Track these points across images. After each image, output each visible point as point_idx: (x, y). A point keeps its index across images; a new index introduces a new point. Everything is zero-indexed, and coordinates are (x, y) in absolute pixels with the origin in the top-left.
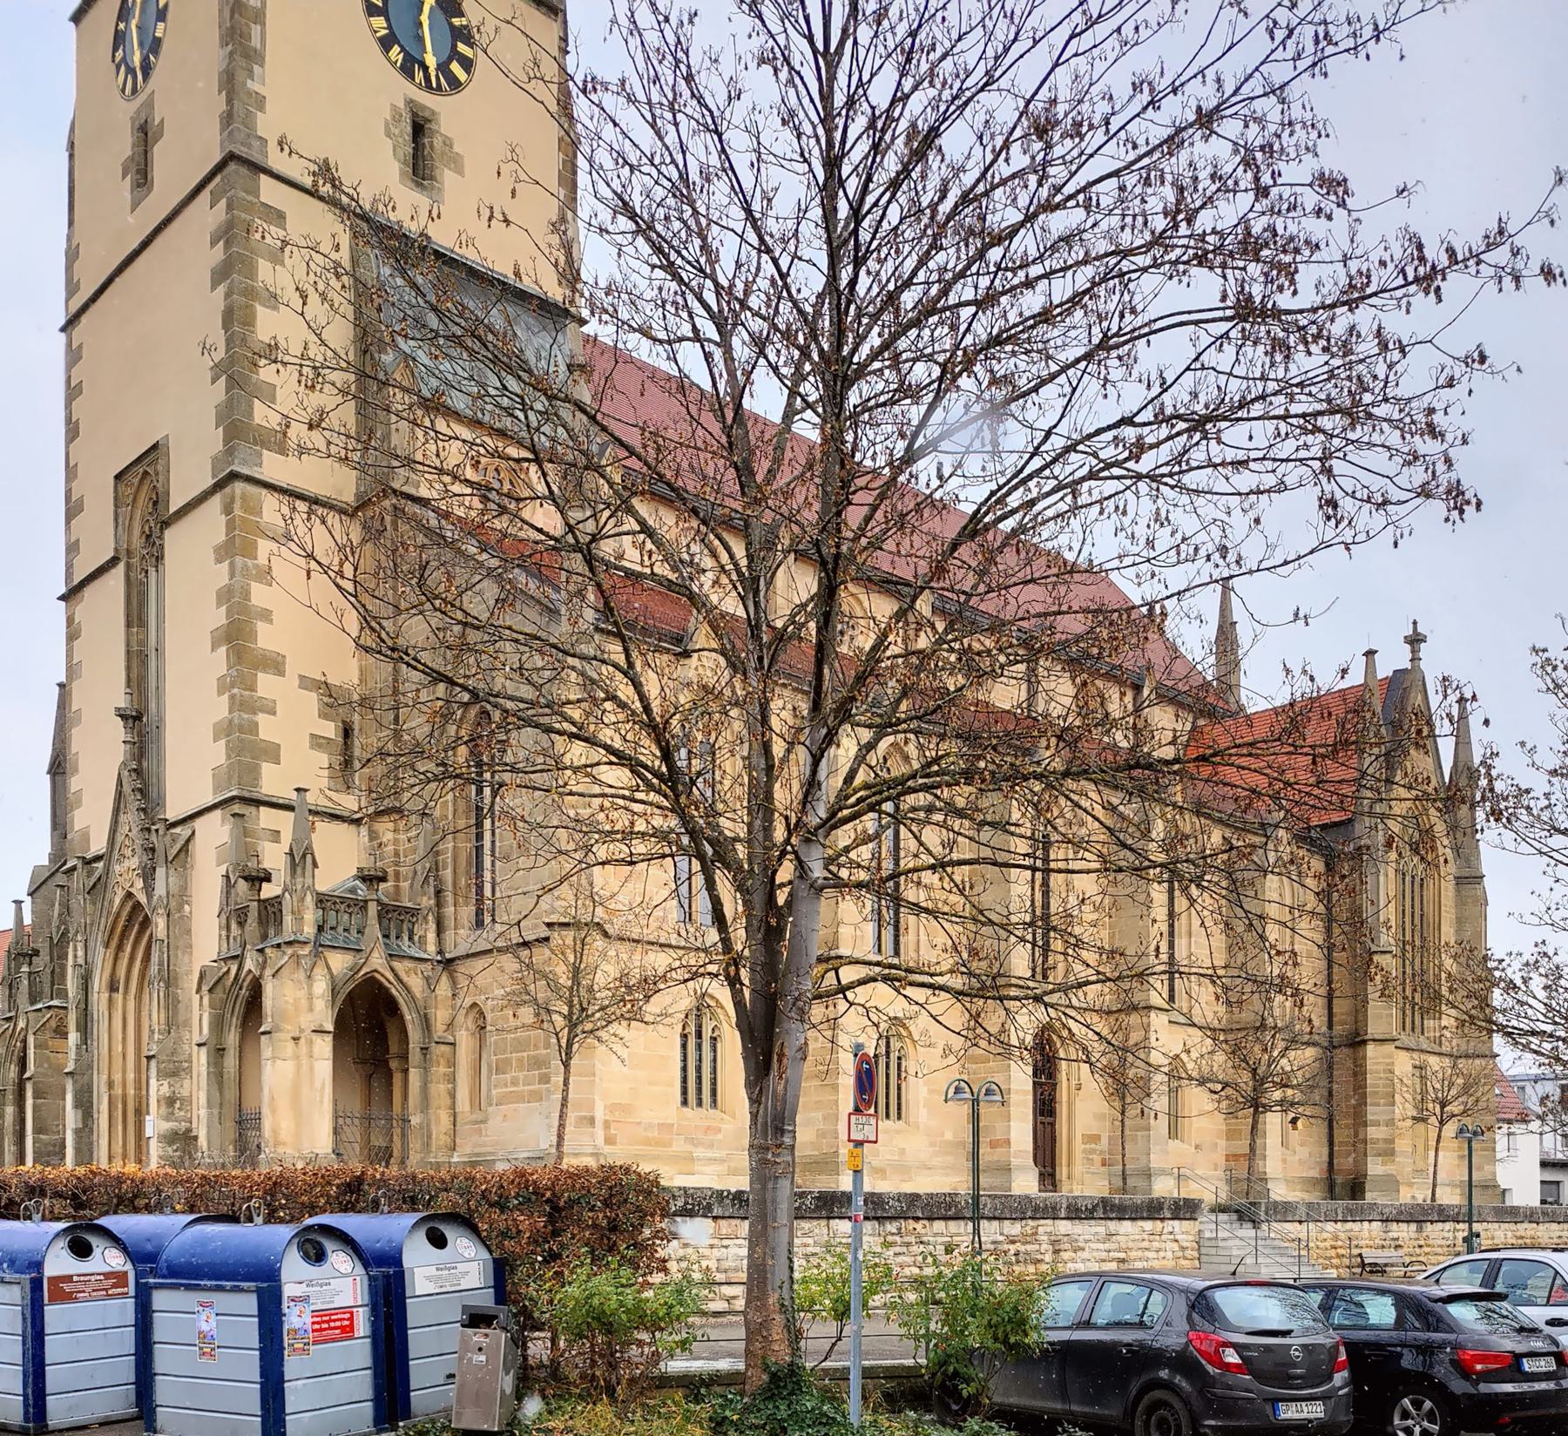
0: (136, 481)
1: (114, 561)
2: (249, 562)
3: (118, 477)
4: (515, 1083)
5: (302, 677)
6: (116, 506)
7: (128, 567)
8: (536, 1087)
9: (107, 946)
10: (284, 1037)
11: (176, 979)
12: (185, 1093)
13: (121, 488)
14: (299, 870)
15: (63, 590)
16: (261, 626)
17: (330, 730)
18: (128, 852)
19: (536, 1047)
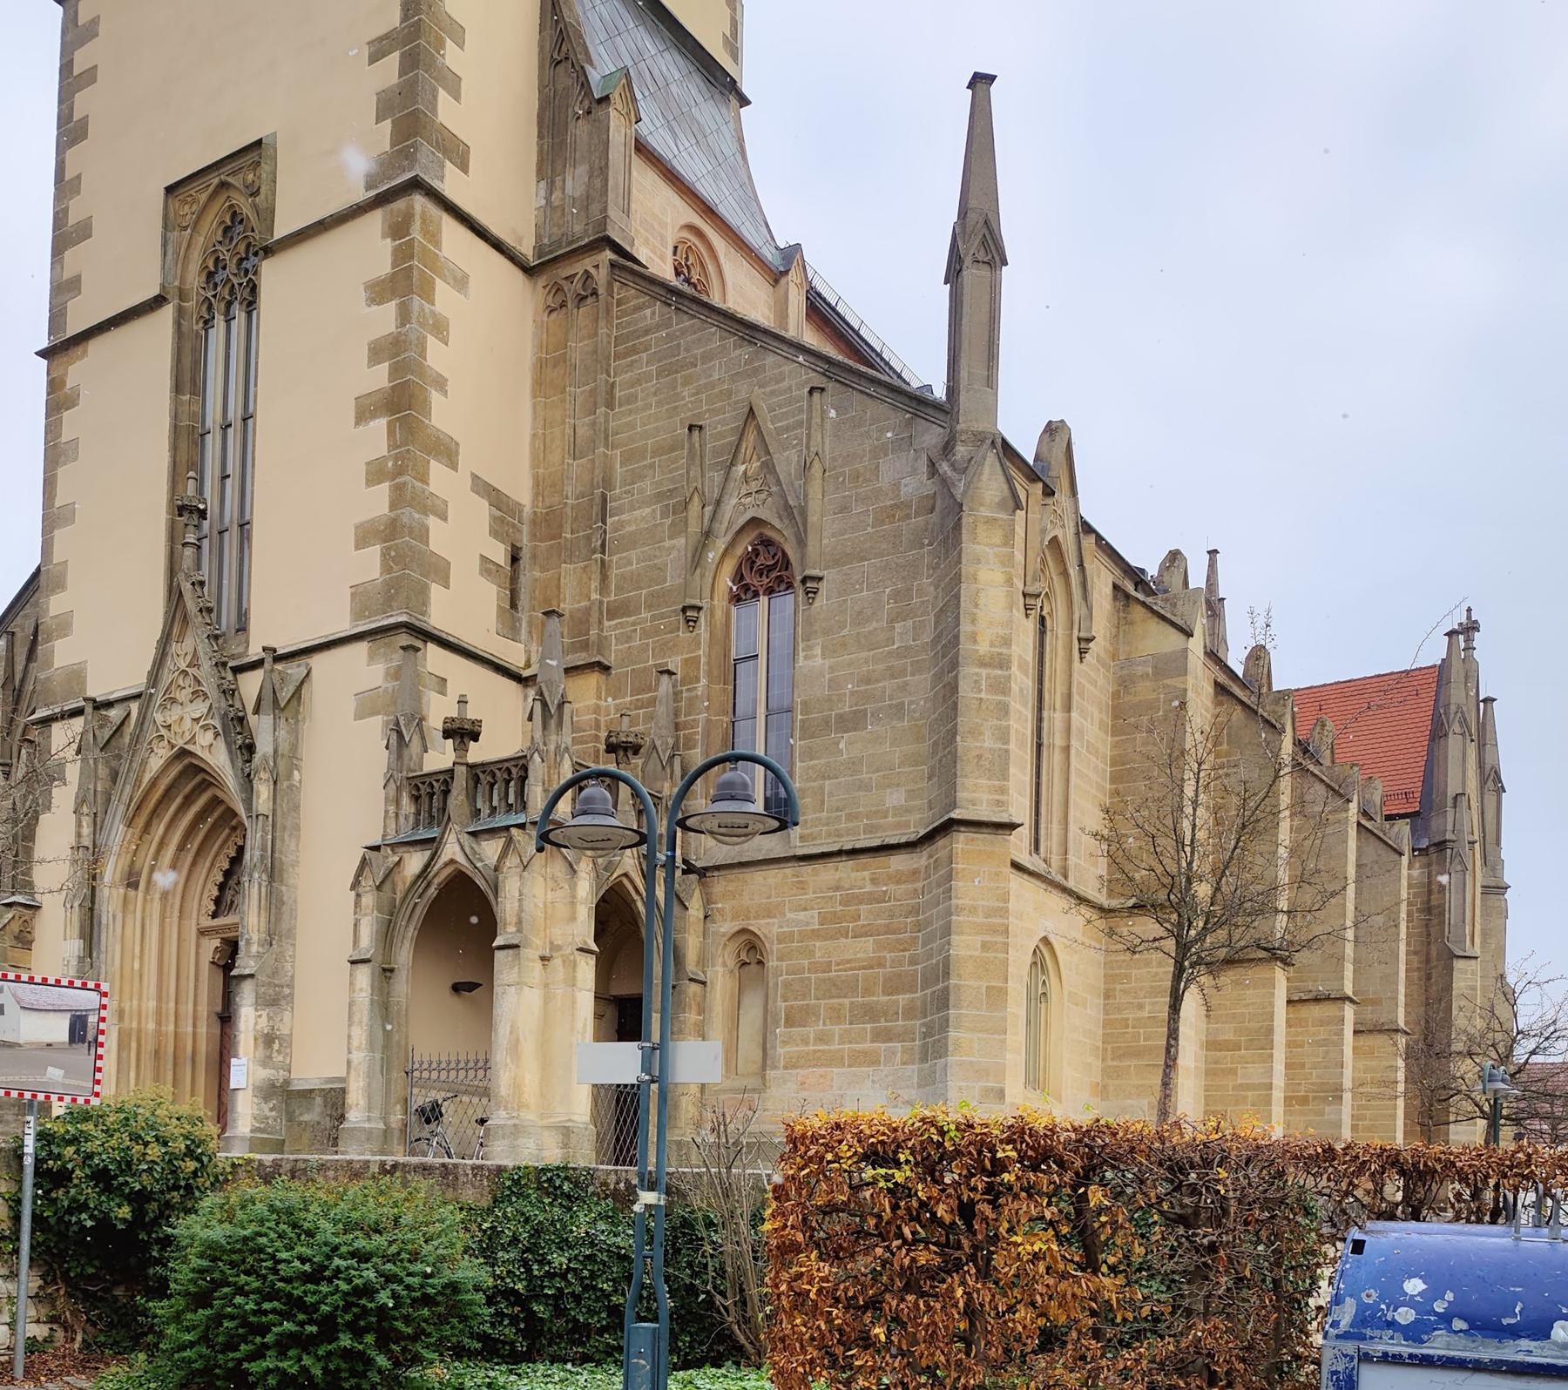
0: (204, 197)
1: (158, 302)
2: (427, 306)
3: (170, 190)
4: (822, 1038)
5: (475, 477)
6: (165, 227)
7: (180, 313)
8: (867, 1046)
9: (129, 825)
10: (531, 954)
11: (281, 870)
12: (285, 1031)
13: (175, 204)
14: (553, 723)
15: (44, 343)
16: (435, 397)
17: (500, 554)
18: (183, 696)
19: (868, 991)
